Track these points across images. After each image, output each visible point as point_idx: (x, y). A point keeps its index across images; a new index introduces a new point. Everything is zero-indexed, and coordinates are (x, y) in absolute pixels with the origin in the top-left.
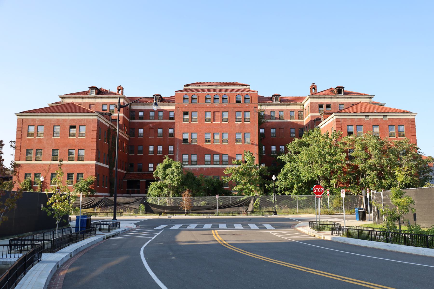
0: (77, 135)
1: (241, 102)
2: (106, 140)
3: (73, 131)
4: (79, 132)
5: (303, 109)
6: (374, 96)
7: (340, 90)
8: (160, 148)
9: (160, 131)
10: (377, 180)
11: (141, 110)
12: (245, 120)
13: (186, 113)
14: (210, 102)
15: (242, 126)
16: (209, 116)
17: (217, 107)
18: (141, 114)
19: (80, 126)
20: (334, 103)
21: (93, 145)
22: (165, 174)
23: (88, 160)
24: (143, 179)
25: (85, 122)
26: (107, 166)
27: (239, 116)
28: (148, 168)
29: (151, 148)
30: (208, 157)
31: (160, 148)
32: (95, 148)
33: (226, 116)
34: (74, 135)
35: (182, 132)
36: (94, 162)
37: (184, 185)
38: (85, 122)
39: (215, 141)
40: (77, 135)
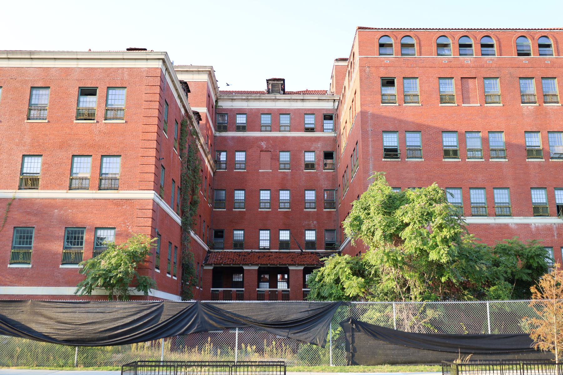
0: (100, 114)
1: (529, 54)
2: (177, 145)
3: (89, 102)
4: (106, 104)
8: (285, 195)
9: (285, 157)
10: (481, 290)
11: (241, 112)
13: (389, 82)
14: (451, 54)
16: (450, 88)
18: (241, 120)
19: (103, 156)
21: (147, 144)
22: (393, 223)
23: (130, 187)
24: (252, 265)
25: (126, 77)
26: (178, 219)
28: (258, 240)
29: (265, 195)
31: (285, 195)
32: (153, 153)
33: (495, 87)
34: (90, 116)
35: (380, 130)
36: (151, 195)
38: (126, 77)
40: (100, 114)
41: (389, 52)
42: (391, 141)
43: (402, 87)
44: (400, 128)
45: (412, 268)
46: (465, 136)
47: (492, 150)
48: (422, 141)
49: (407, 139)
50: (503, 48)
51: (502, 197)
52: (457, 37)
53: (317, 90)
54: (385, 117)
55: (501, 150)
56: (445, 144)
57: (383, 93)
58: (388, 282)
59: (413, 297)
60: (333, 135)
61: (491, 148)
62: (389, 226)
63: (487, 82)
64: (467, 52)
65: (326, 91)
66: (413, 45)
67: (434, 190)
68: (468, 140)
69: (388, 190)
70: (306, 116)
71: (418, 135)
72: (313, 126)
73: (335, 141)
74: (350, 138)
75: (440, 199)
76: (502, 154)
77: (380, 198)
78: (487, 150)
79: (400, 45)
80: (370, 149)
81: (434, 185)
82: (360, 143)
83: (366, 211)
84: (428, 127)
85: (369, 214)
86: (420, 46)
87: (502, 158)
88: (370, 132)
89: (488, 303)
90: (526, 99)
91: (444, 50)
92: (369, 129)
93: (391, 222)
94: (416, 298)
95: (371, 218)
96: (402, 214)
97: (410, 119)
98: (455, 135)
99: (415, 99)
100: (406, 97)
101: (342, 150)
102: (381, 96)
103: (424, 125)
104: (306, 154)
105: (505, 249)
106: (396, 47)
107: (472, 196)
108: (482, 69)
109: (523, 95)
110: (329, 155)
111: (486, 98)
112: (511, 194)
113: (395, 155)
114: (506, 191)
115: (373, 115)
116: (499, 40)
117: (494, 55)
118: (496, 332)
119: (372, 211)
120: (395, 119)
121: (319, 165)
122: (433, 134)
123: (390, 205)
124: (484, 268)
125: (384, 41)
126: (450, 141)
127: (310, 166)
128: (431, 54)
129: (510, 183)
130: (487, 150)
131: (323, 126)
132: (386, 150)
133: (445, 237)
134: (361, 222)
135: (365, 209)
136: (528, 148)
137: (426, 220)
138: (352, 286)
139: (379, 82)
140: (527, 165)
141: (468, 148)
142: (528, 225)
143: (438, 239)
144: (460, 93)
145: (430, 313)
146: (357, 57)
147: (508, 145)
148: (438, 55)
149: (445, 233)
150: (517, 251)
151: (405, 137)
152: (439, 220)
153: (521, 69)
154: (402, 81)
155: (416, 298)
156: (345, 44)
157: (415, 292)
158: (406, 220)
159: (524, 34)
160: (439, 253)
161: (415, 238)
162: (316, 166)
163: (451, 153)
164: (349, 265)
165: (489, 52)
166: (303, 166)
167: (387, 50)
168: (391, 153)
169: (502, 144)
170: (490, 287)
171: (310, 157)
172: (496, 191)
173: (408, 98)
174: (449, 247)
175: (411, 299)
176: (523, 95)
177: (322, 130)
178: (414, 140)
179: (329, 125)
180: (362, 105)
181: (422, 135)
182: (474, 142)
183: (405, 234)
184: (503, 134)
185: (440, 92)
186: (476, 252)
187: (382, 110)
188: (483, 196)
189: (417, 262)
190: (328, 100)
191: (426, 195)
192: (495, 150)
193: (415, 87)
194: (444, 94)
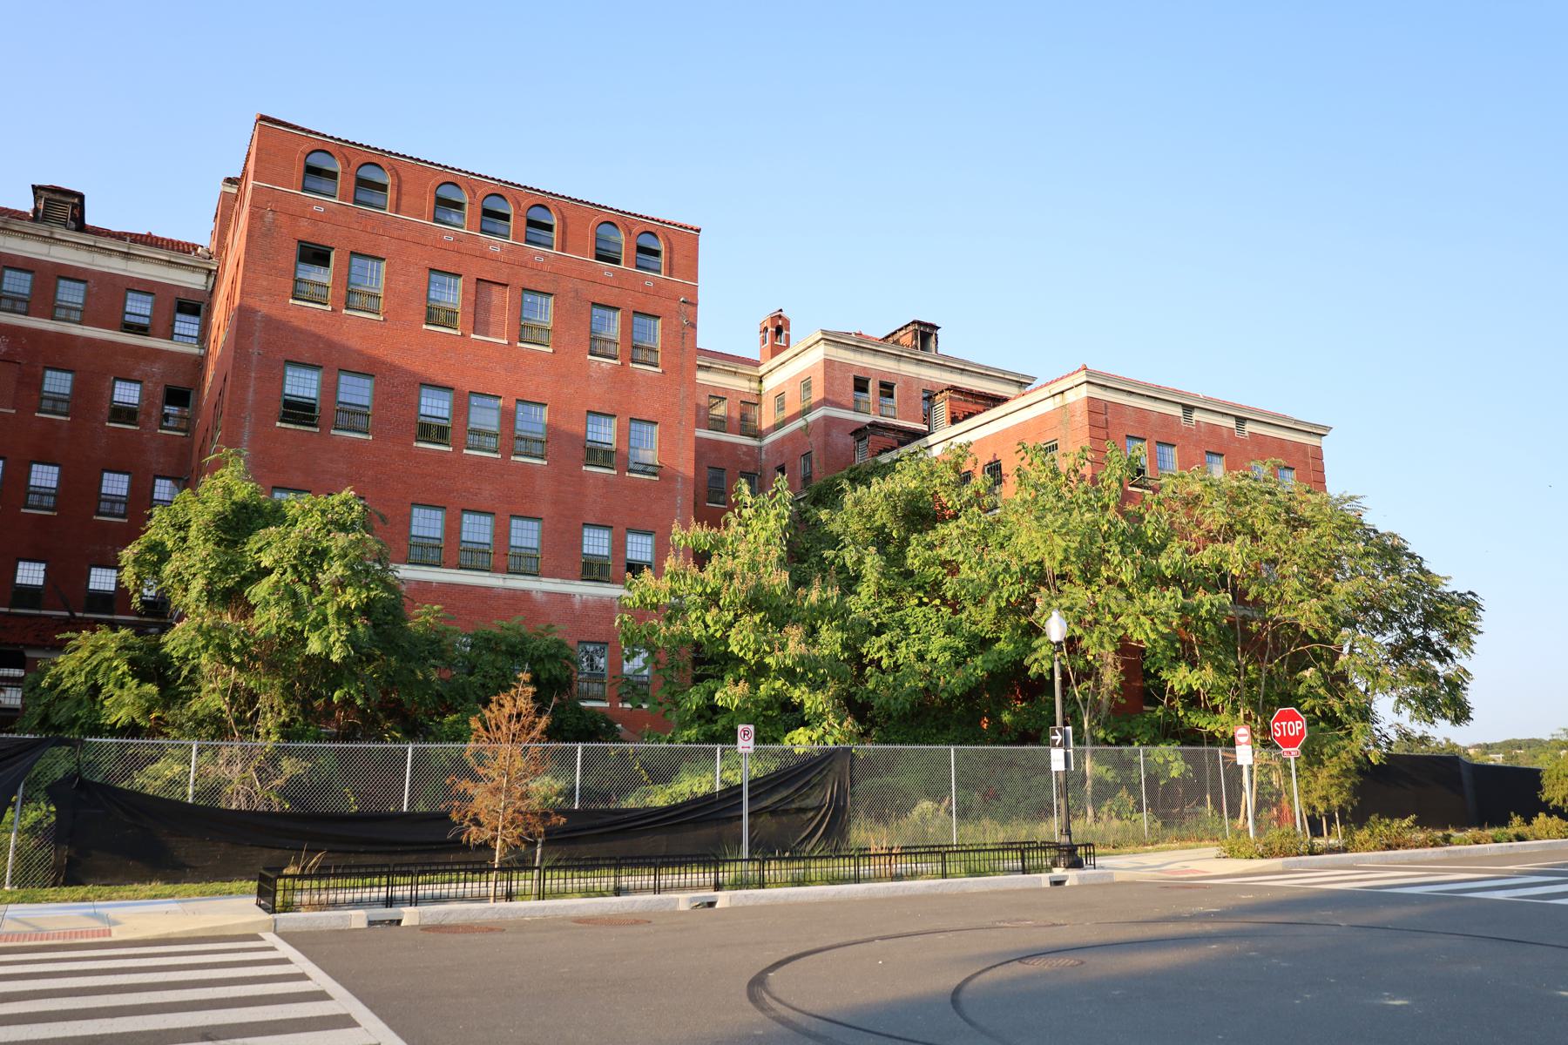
1: (617, 262)
5: (759, 395)
6: (1034, 379)
7: (925, 333)
12: (635, 351)
13: (316, 255)
14: (462, 226)
15: (620, 378)
16: (451, 295)
17: (494, 259)
20: (908, 381)
22: (237, 565)
27: (613, 326)
30: (427, 524)
33: (544, 313)
37: (850, 586)
39: (641, 355)
41: (315, 186)
42: (302, 385)
43: (345, 271)
44: (331, 360)
45: (272, 667)
46: (468, 401)
47: (519, 438)
48: (375, 397)
49: (342, 388)
50: (569, 238)
51: (525, 535)
52: (480, 193)
53: (175, 238)
54: (296, 330)
55: (536, 441)
56: (423, 411)
57: (300, 276)
58: (211, 699)
59: (262, 731)
60: (195, 350)
61: (518, 433)
62: (225, 572)
63: (528, 298)
64: (502, 230)
65: (195, 247)
66: (383, 188)
67: (344, 503)
68: (472, 410)
69: (243, 492)
70: (130, 295)
71: (368, 383)
72: (146, 321)
73: (199, 363)
74: (220, 362)
75: (353, 523)
76: (537, 448)
77: (215, 505)
78: (509, 438)
79: (353, 179)
80: (251, 396)
81: (348, 493)
82: (229, 378)
83: (182, 534)
84: (393, 368)
85: (184, 540)
86: (399, 192)
87: (536, 457)
88: (254, 358)
89: (580, 746)
90: (599, 347)
91: (450, 213)
92: (255, 351)
93: (231, 562)
94: (268, 733)
95: (1154, 579)
96: (269, 548)
97: (355, 343)
98: (448, 395)
99: (372, 303)
100: (349, 297)
101: (207, 391)
102: (291, 283)
103: (383, 363)
104: (118, 384)
105: (488, 640)
106: (345, 183)
107: (465, 527)
108: (523, 270)
109: (595, 339)
110: (178, 396)
111: (523, 331)
112: (543, 531)
113: (306, 417)
114: (535, 525)
115: (269, 321)
116: (563, 219)
117: (551, 247)
118: (421, 807)
119: (193, 532)
120: (319, 337)
121: (149, 415)
122: (401, 387)
123: (238, 524)
124: (870, 686)
125: (318, 161)
126: (435, 406)
127: (125, 413)
128: (421, 216)
129: (545, 510)
130: (509, 438)
131: (173, 326)
132: (288, 404)
133: (347, 606)
134: (164, 556)
135: (180, 528)
136: (589, 445)
137: (310, 566)
138: (124, 702)
139: (293, 250)
140: (583, 477)
141: (472, 426)
142: (568, 596)
143: (331, 610)
144: (471, 310)
145: (288, 766)
146: (251, 183)
147: (551, 429)
148: (436, 220)
149: (348, 597)
150: (513, 646)
151: (337, 382)
152: (337, 569)
153: (598, 287)
154: (346, 258)
155: (268, 733)
156: (232, 151)
157: (268, 722)
158: (266, 561)
159: (614, 220)
160: (327, 637)
161: (277, 604)
162: (140, 418)
163: (434, 432)
164: (128, 654)
165: (542, 240)
166: (106, 411)
167: (324, 184)
168: (298, 411)
169: (540, 429)
170: (443, 715)
171: (127, 394)
172: (514, 522)
173: (356, 298)
174: (354, 627)
175: (257, 736)
176: (595, 339)
177: (170, 335)
178: (356, 391)
179: (186, 326)
180: (242, 297)
181: (376, 384)
182: (485, 417)
183: (259, 592)
184: (545, 410)
185: (428, 299)
186: (432, 642)
187: (291, 313)
188: (488, 530)
189: (279, 655)
190: (194, 269)
191: (323, 512)
192: (526, 439)
193: (374, 277)
194: (436, 304)
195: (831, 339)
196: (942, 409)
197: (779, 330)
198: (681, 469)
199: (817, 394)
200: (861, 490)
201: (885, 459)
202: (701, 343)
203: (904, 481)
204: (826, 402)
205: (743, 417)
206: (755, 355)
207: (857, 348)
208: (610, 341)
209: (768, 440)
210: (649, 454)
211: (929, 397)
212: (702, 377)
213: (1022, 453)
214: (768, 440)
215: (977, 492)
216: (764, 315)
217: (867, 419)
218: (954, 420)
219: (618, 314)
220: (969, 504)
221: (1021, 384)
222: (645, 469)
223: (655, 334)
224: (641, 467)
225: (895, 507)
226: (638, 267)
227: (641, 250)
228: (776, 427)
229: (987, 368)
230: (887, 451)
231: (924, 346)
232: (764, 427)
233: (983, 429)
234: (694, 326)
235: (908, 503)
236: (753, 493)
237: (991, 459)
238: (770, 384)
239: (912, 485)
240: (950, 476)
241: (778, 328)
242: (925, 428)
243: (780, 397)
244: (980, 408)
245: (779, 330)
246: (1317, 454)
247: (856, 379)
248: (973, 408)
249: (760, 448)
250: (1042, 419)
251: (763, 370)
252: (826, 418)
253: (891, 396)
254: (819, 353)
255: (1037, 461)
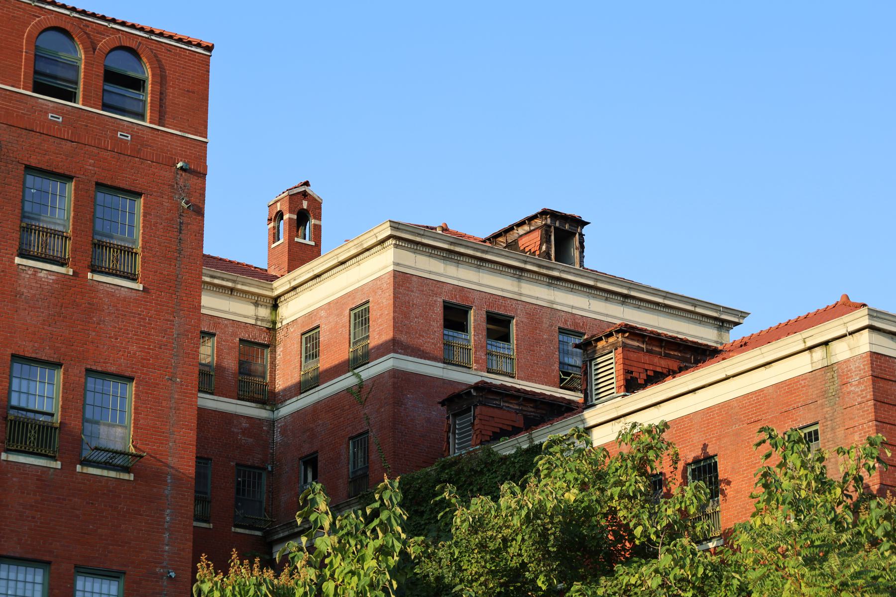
1: (70, 96)
5: (272, 330)
6: (743, 315)
12: (97, 252)
15: (72, 298)
20: (535, 312)
27: (60, 209)
195: (405, 237)
196: (609, 366)
197: (302, 218)
198: (171, 461)
199: (381, 331)
200: (479, 504)
201: (506, 448)
202: (210, 248)
203: (554, 490)
204: (394, 346)
205: (245, 369)
206: (260, 261)
207: (449, 256)
208: (55, 234)
209: (286, 410)
210: (118, 434)
211: (588, 347)
212: (211, 303)
213: (766, 448)
214: (286, 410)
215: (684, 513)
216: (276, 189)
217: (470, 378)
218: (631, 386)
219: (70, 187)
220: (672, 533)
221: (723, 325)
222: (113, 459)
223: (134, 223)
224: (103, 457)
225: (544, 535)
226: (106, 107)
227: (111, 77)
228: (302, 387)
229: (667, 295)
230: (514, 432)
231: (562, 255)
232: (281, 384)
233: (679, 402)
234: (199, 211)
235: (565, 527)
236: (336, 508)
237: (697, 452)
238: (292, 311)
239: (571, 496)
240: (636, 483)
241: (301, 212)
242: (576, 397)
243: (311, 340)
244: (674, 365)
245: (302, 218)
246: (488, 323)
247: (448, 308)
248: (661, 364)
249: (272, 423)
250: (789, 386)
251: (280, 286)
252: (396, 374)
253: (506, 338)
254: (383, 262)
255: (793, 460)
